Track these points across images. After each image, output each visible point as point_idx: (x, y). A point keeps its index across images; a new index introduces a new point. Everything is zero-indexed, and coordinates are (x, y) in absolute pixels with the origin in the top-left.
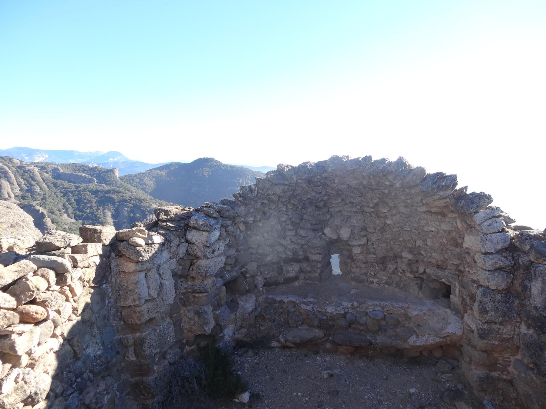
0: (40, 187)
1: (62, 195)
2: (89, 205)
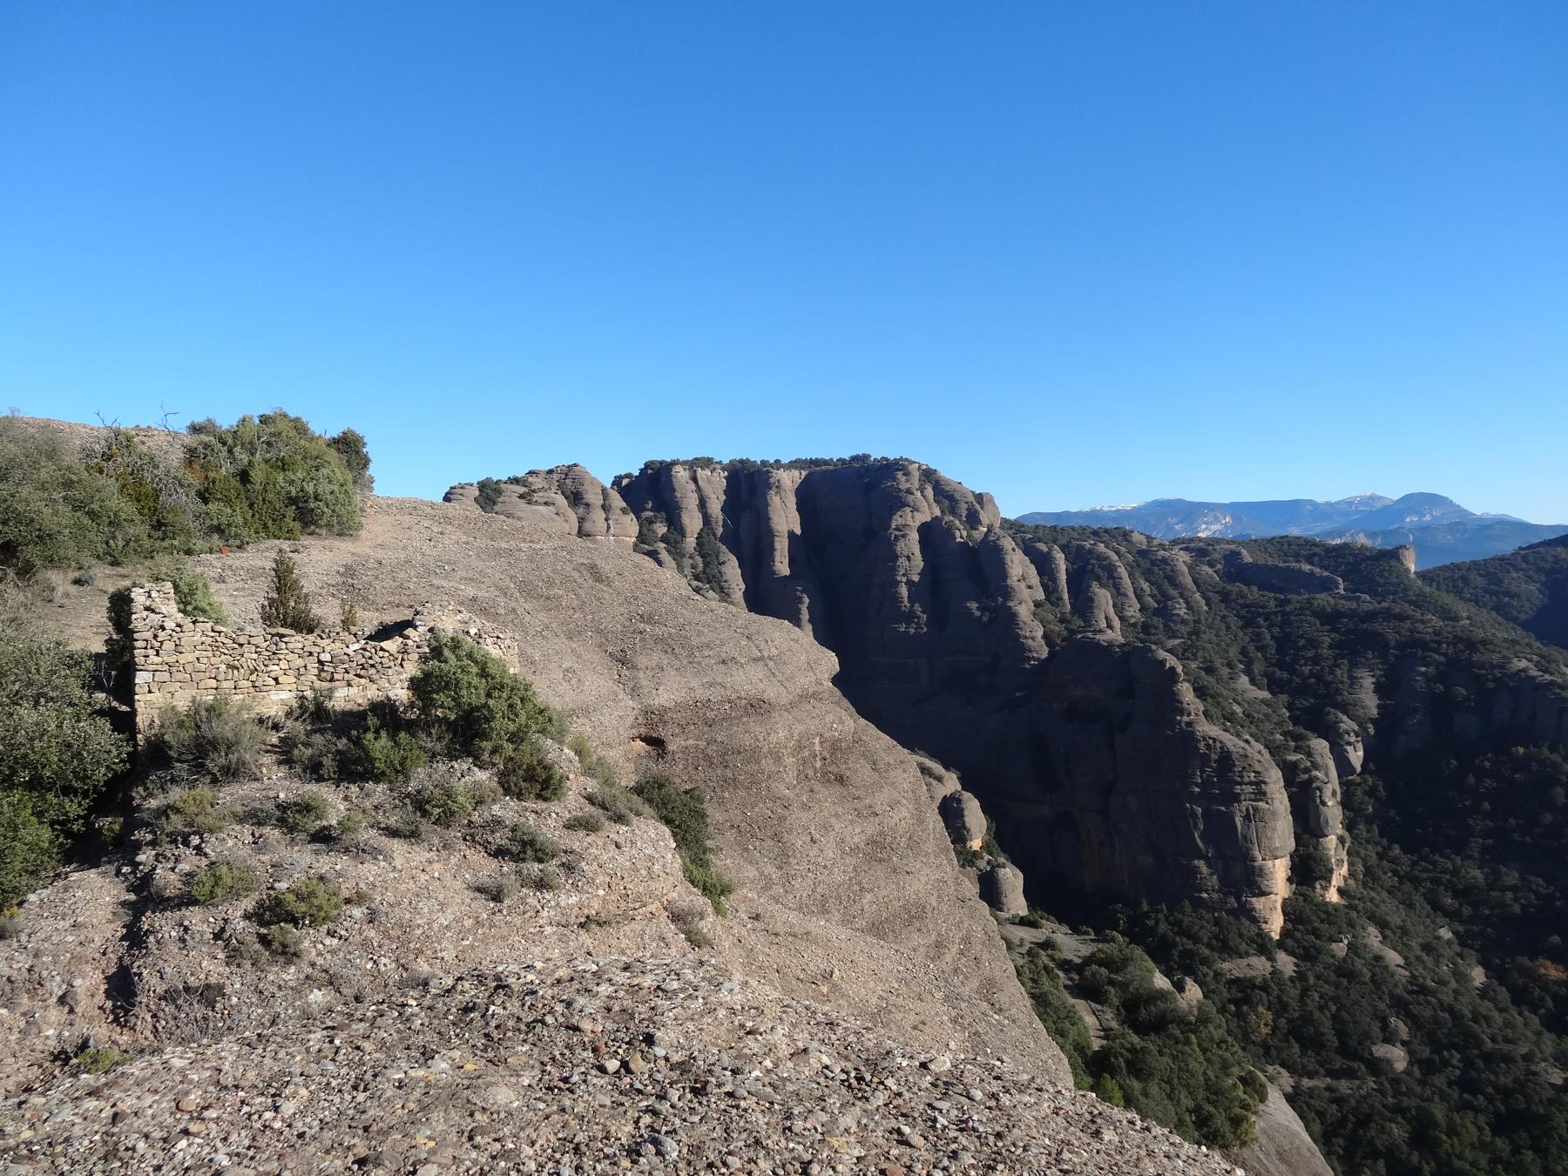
0: (1187, 602)
2: (1310, 654)
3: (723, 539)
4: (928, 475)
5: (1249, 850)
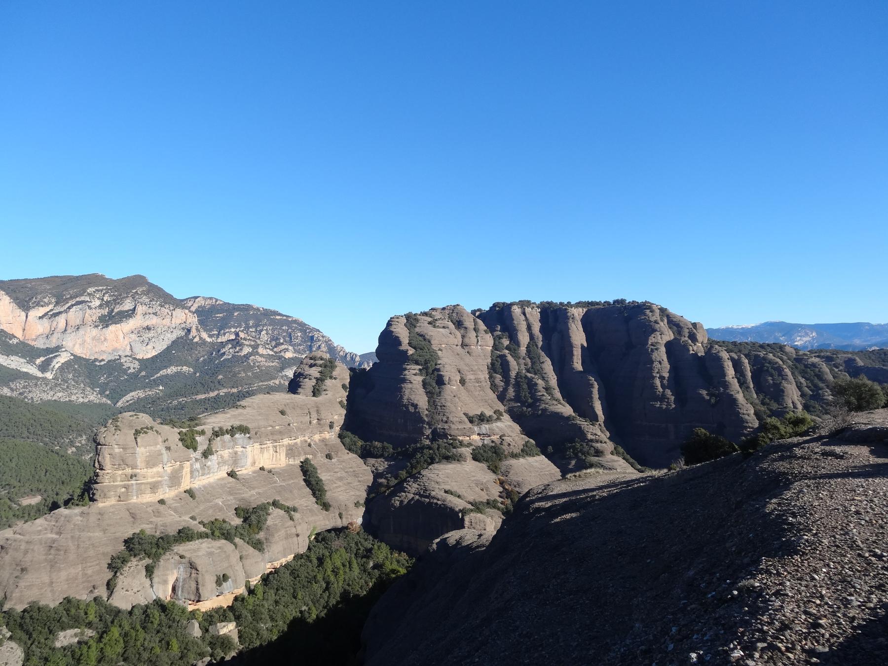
4: (663, 311)
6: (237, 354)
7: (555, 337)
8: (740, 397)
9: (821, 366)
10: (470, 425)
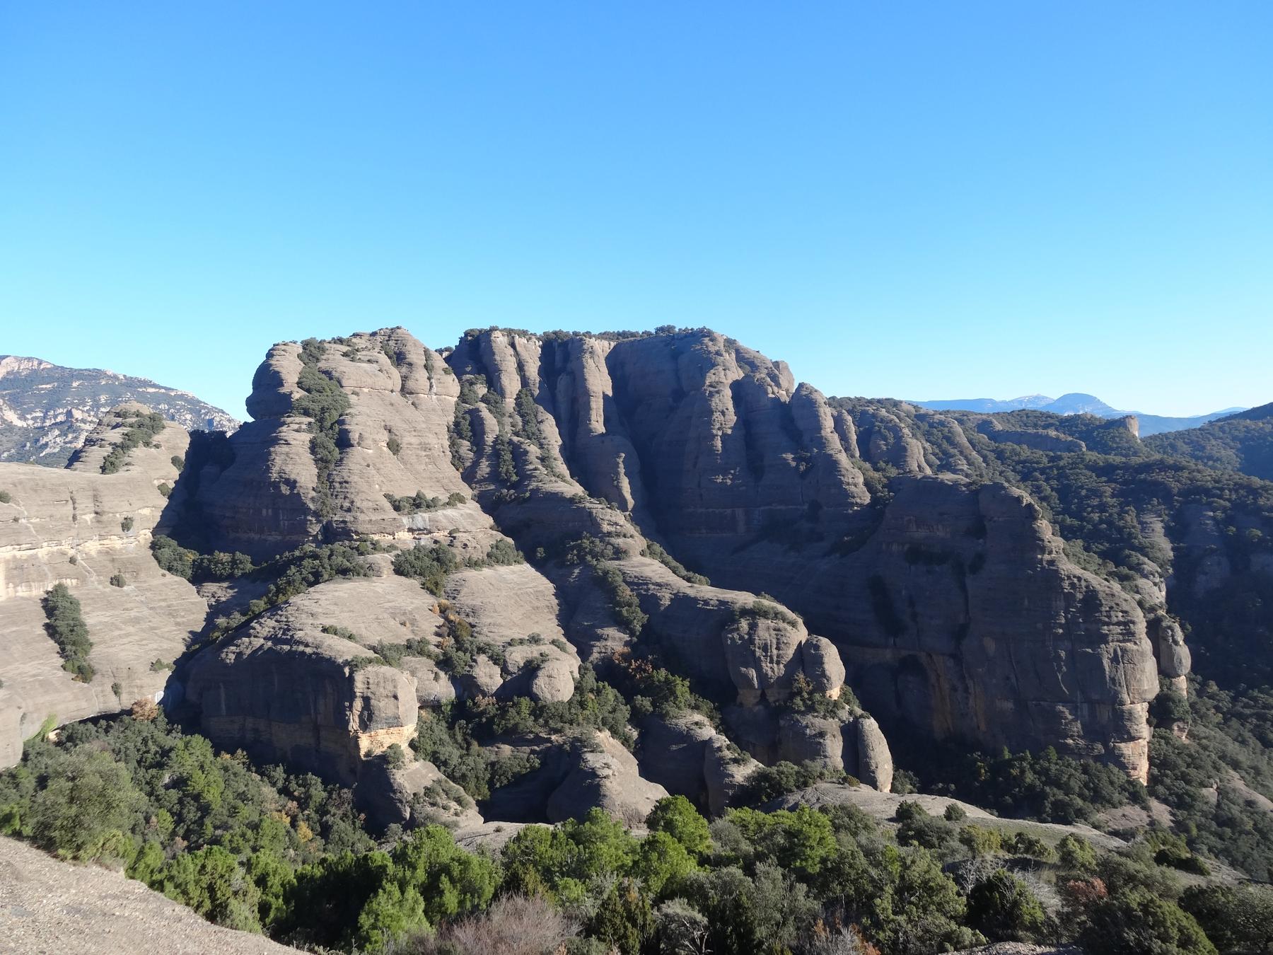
0: (966, 458)
1: (1018, 478)
2: (1096, 502)
3: (538, 400)
4: (730, 343)
5: (1117, 693)
6: (69, 445)
7: (562, 382)
8: (843, 458)
9: (952, 425)
10: (395, 514)
